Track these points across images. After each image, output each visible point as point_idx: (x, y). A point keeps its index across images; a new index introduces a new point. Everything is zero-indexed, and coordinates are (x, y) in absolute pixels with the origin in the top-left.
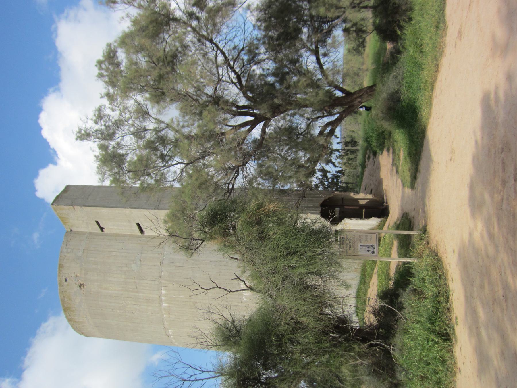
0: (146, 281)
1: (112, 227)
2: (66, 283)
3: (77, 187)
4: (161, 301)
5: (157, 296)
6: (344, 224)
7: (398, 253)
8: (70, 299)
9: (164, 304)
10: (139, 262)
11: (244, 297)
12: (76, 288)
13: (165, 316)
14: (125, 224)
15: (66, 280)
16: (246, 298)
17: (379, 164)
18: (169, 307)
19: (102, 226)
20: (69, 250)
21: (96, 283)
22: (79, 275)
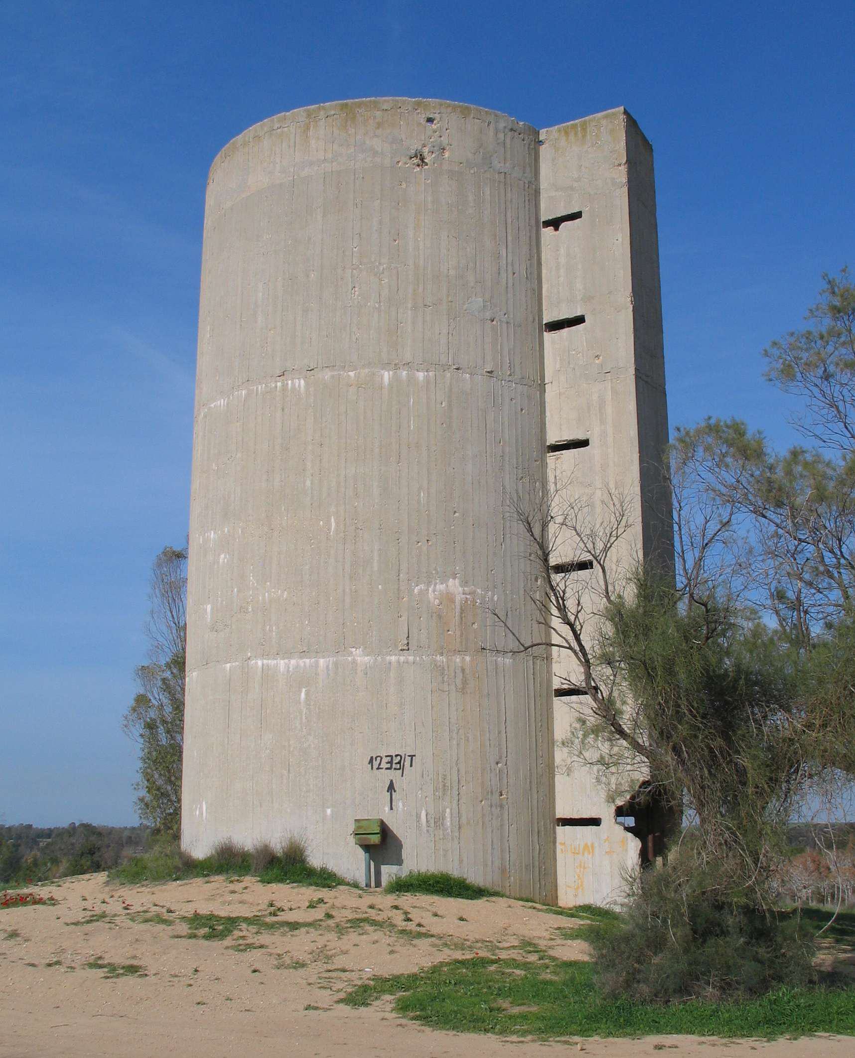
0: (445, 331)
1: (562, 251)
2: (423, 121)
3: (201, 247)
4: (396, 367)
5: (408, 357)
6: (624, 842)
7: (610, 1034)
8: (379, 125)
9: (387, 376)
10: (488, 315)
11: (422, 586)
12: (415, 146)
13: (352, 374)
14: (579, 286)
15: (430, 120)
16: (421, 591)
17: (193, 400)
18: (381, 388)
19: (563, 225)
20: (501, 136)
21: (430, 199)
22: (447, 154)
